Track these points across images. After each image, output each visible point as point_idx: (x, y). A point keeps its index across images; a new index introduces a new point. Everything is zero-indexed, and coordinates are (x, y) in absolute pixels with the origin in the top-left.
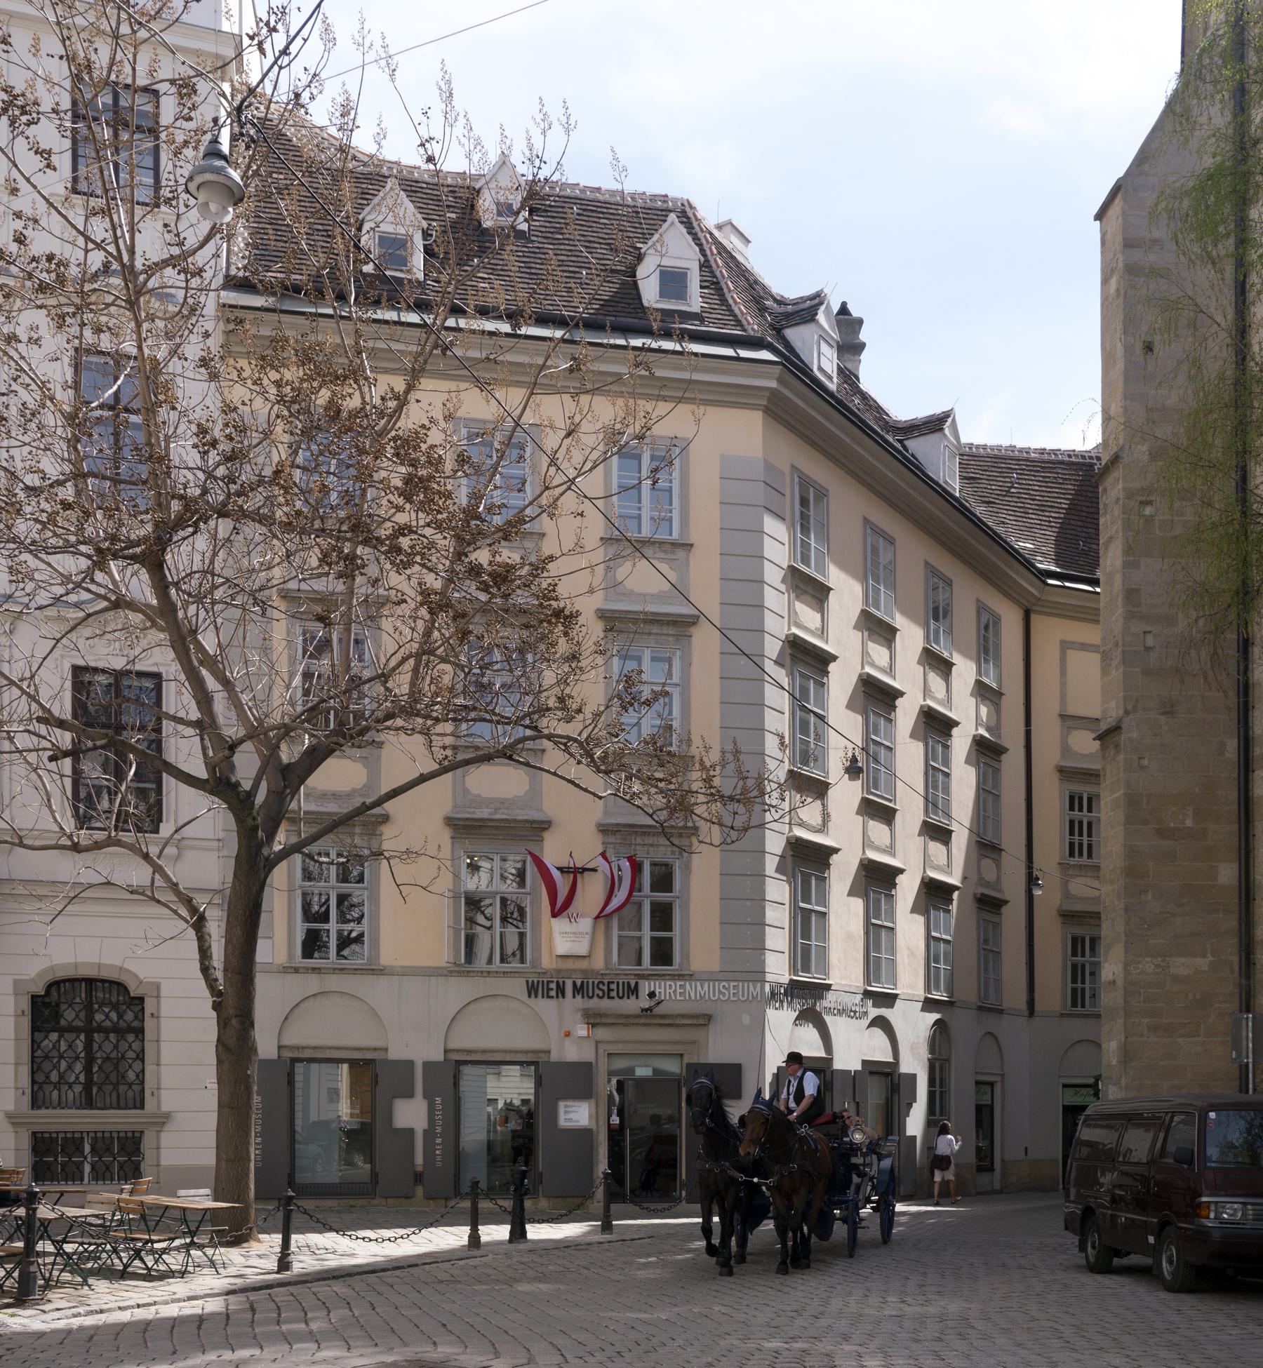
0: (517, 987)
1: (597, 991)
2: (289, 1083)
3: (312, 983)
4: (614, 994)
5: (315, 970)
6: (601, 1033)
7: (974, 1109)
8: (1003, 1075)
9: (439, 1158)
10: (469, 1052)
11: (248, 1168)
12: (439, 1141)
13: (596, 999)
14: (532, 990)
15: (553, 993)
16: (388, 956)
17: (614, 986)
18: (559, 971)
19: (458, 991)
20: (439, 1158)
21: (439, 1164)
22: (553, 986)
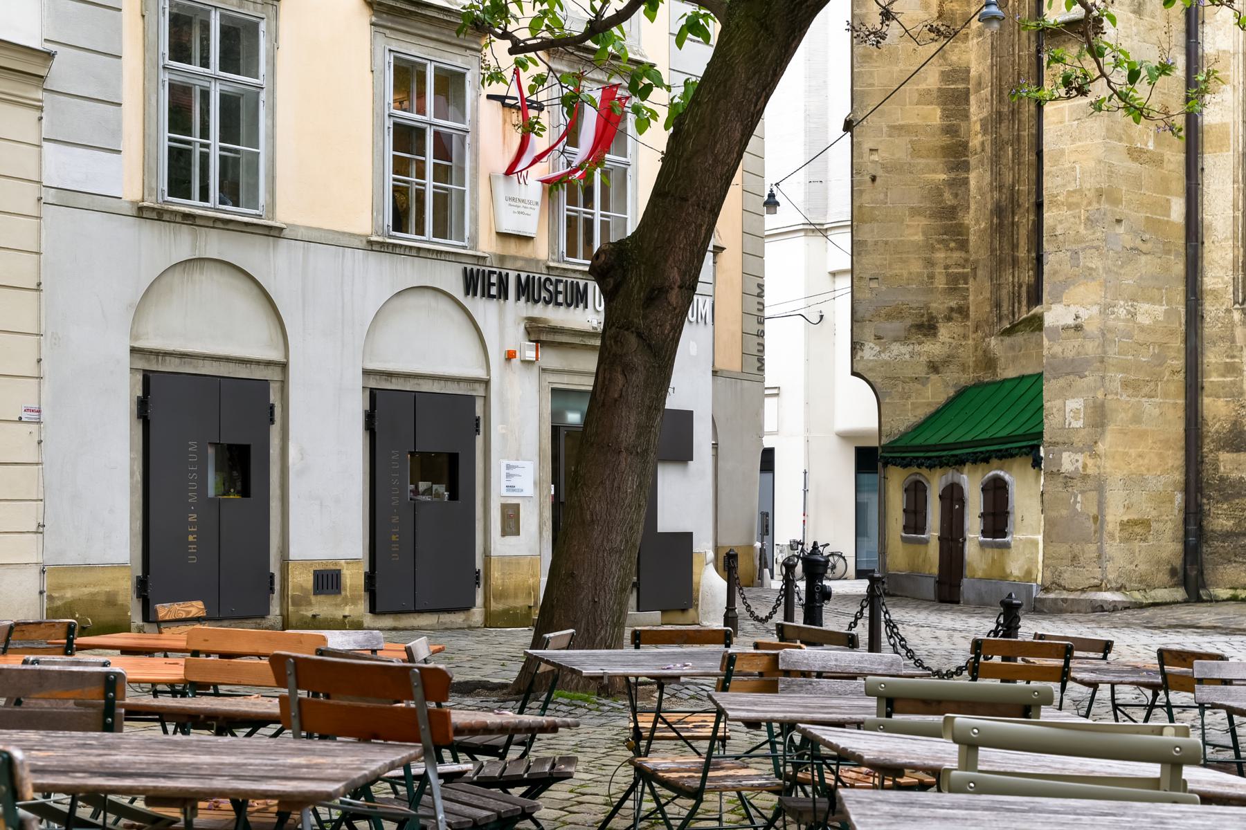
0: (450, 278)
1: (544, 294)
2: (1215, 627)
3: (182, 244)
4: (561, 298)
5: (189, 219)
6: (551, 359)
7: (357, 405)
8: (284, 366)
9: (192, 549)
10: (390, 375)
11: (59, 672)
12: (193, 517)
13: (540, 305)
14: (475, 282)
15: (494, 291)
16: (288, 210)
17: (561, 288)
18: (502, 258)
19: (382, 277)
20: (192, 549)
21: (193, 560)
22: (494, 279)
